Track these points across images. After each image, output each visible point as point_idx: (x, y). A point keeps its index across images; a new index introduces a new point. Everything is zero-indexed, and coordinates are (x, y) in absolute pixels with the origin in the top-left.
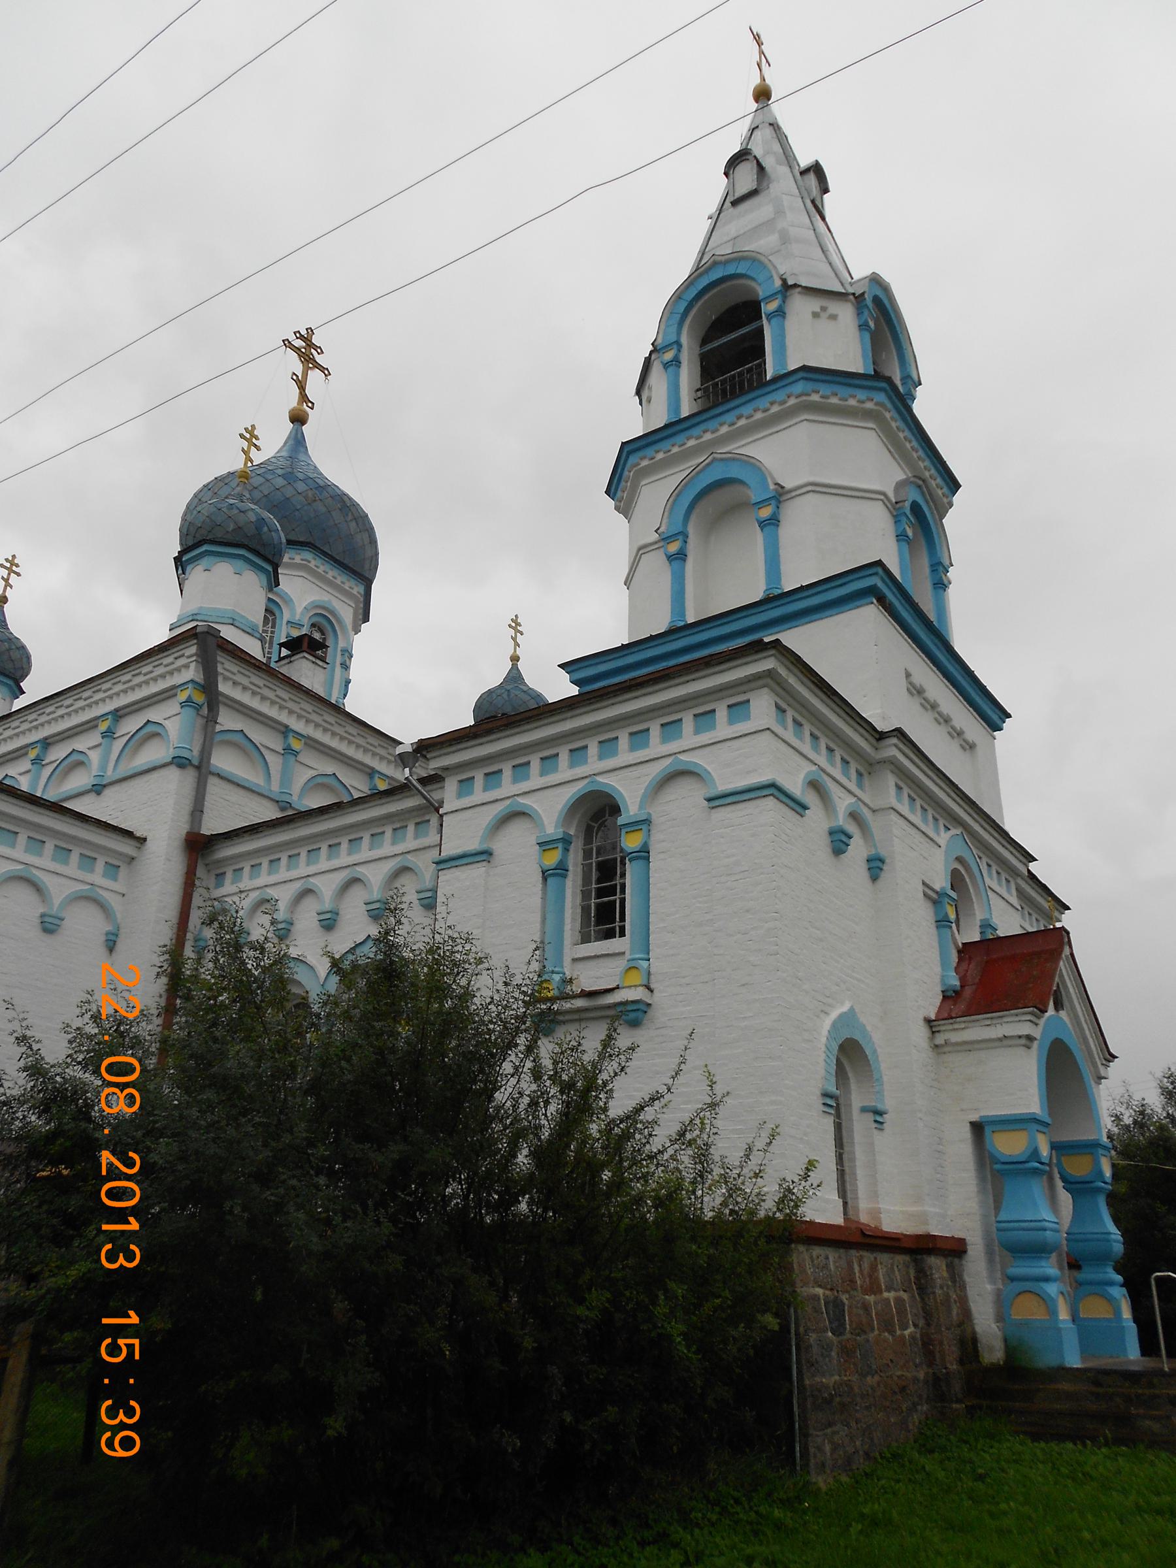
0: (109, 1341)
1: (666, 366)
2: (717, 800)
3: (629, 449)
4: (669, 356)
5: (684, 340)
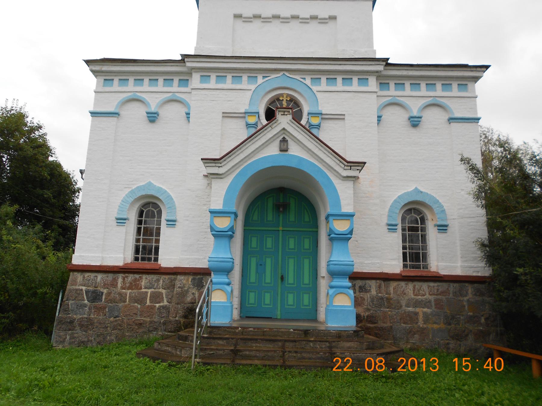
0: (463, 369)
2: (452, 120)
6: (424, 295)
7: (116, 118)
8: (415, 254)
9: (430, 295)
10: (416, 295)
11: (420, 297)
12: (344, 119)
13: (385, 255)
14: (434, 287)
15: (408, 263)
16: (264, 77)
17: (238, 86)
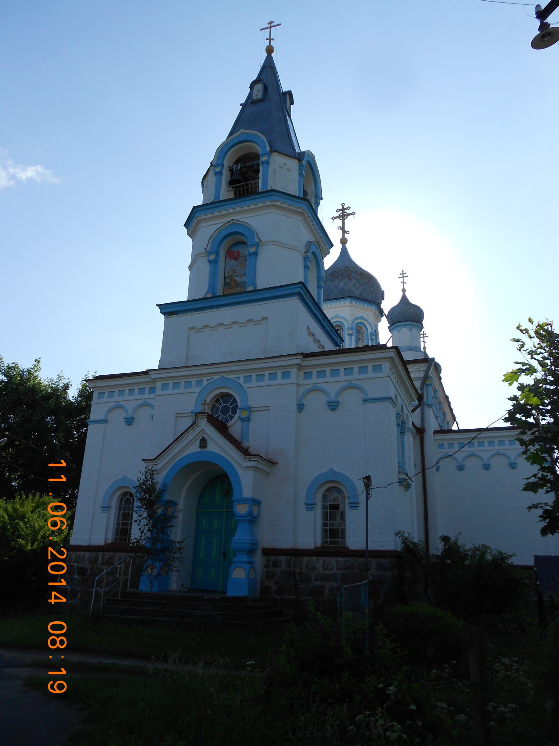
1: (216, 173)
2: (366, 401)
3: (195, 209)
4: (218, 169)
5: (225, 164)
6: (331, 570)
7: (104, 424)
8: (333, 530)
9: (338, 569)
10: (324, 570)
11: (328, 571)
12: (298, 405)
13: (307, 533)
14: (341, 561)
15: (329, 539)
16: (208, 380)
17: (189, 390)
